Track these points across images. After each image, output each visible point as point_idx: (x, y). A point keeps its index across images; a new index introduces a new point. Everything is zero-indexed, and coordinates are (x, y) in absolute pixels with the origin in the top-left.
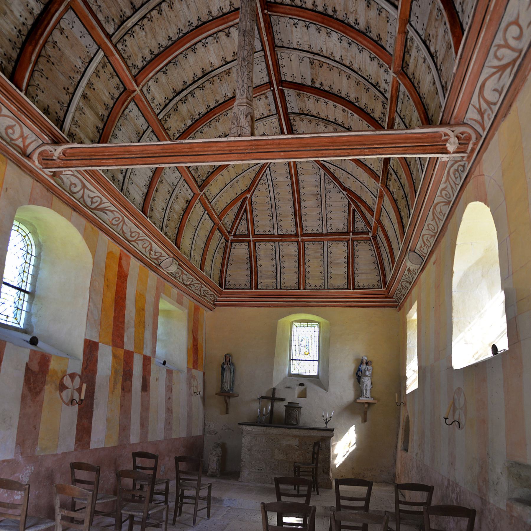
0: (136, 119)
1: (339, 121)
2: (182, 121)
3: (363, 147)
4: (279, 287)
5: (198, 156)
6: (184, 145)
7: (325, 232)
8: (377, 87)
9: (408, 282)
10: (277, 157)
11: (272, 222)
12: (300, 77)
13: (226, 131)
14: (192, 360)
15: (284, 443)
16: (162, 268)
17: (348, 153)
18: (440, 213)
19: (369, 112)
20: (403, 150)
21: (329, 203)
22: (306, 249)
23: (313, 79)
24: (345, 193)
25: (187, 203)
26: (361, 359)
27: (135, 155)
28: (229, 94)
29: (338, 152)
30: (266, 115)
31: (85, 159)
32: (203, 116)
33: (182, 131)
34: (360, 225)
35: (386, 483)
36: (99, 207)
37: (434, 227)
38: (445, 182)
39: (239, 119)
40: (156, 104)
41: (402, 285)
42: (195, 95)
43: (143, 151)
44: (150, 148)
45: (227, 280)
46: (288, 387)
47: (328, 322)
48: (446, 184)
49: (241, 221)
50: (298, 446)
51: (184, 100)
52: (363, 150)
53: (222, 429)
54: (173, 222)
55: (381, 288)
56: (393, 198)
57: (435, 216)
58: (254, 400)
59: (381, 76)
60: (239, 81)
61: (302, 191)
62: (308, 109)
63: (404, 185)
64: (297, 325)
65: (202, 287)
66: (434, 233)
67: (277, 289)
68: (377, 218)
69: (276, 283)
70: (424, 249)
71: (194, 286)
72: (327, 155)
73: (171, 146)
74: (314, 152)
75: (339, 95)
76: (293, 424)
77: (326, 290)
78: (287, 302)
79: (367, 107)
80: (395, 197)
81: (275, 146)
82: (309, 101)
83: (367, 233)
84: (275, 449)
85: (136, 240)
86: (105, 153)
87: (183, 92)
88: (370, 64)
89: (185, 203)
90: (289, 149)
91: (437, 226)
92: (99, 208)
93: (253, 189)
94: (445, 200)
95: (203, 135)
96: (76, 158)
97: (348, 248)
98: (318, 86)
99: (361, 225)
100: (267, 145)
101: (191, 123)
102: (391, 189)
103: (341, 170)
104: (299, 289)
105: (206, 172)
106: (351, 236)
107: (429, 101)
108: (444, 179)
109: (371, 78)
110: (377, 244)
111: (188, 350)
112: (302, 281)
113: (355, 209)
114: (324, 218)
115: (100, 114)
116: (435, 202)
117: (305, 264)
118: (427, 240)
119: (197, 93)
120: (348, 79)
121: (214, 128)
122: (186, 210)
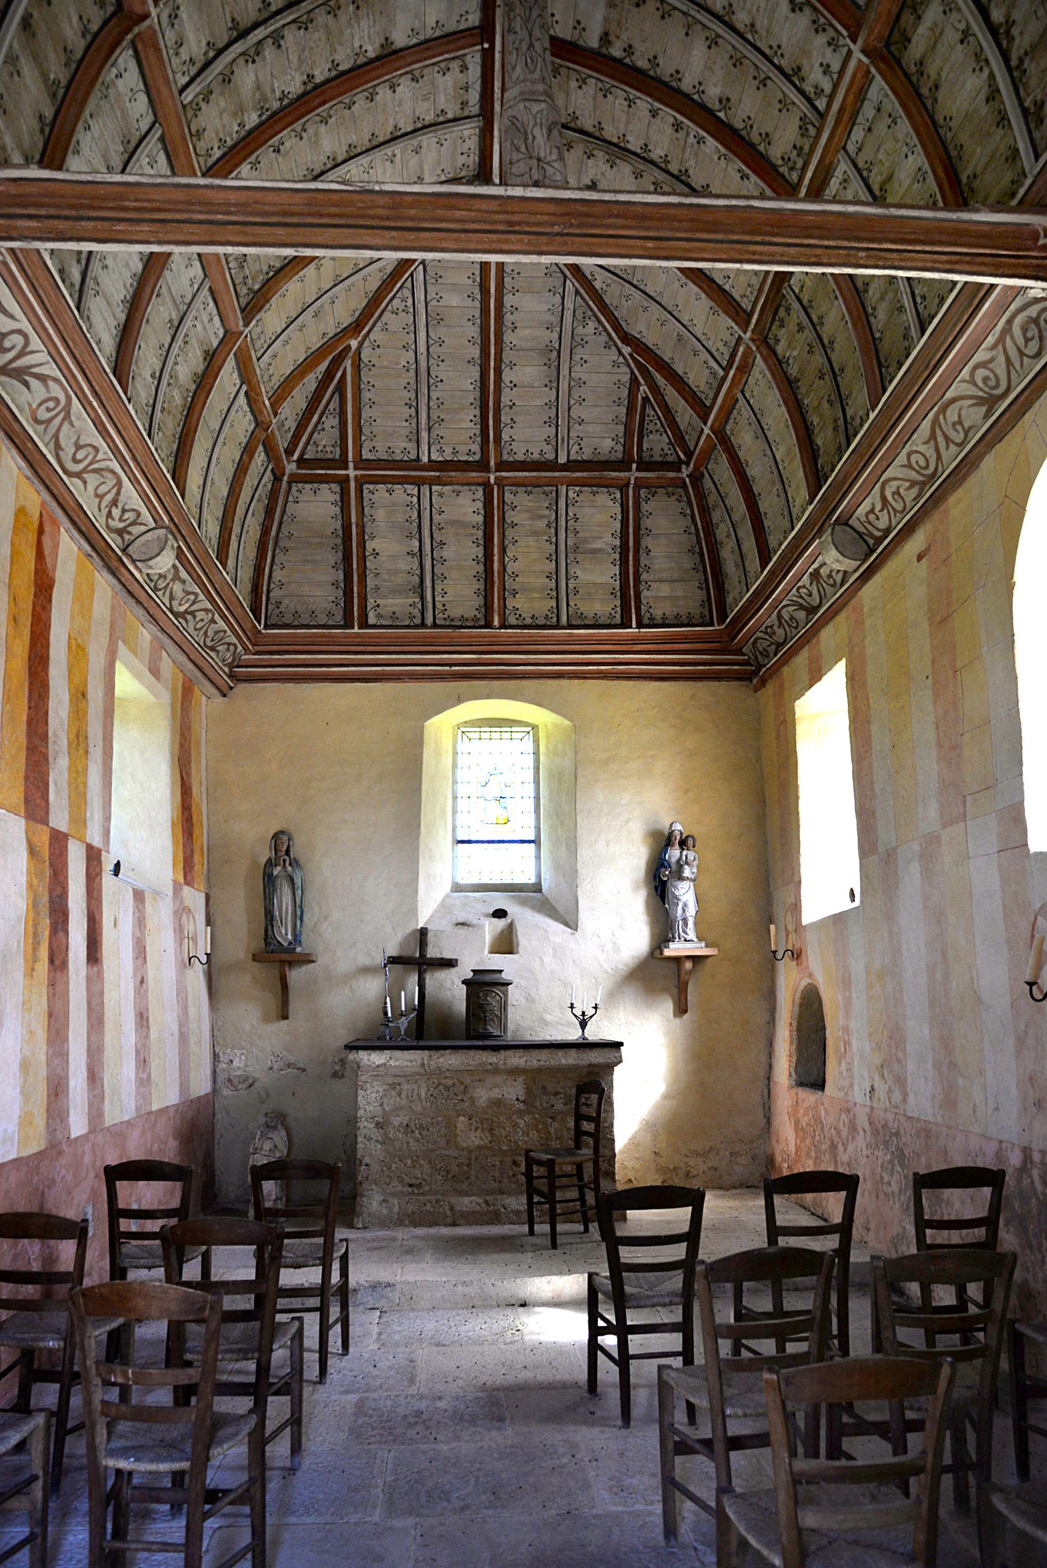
0: (127, 100)
1: (657, 154)
2: (235, 114)
3: (857, 245)
4: (429, 621)
5: (417, 233)
6: (375, 196)
7: (562, 459)
8: (795, 80)
9: (801, 607)
10: (635, 253)
11: (414, 425)
12: (571, 22)
13: (339, 152)
14: (181, 858)
15: (483, 1095)
16: (133, 561)
17: (817, 256)
18: (954, 424)
19: (755, 138)
20: (947, 262)
21: (578, 375)
22: (506, 508)
23: (606, 34)
24: (626, 350)
25: (205, 359)
26: (666, 832)
27: (224, 214)
28: (370, 48)
29: (792, 250)
30: (450, 116)
31: (58, 217)
32: (290, 104)
33: (229, 143)
34: (658, 443)
35: (742, 1186)
36: (14, 365)
37: (927, 461)
38: (994, 347)
39: (530, 137)
40: (184, 58)
41: (780, 616)
42: (282, 43)
43: (246, 205)
44: (270, 197)
45: (272, 600)
46: (463, 924)
47: (567, 722)
48: (994, 352)
49: (324, 419)
50: (523, 1102)
51: (251, 57)
52: (853, 252)
53: (271, 1069)
54: (171, 417)
55: (713, 625)
56: (785, 373)
57: (938, 431)
58: (367, 970)
59: (815, 53)
60: (518, 29)
61: (508, 337)
62: (570, 111)
63: (831, 343)
64: (471, 735)
65: (213, 621)
66: (923, 475)
67: (423, 625)
68: (716, 426)
69: (419, 606)
70: (878, 519)
71: (195, 617)
72: (765, 258)
73: (335, 197)
74: (734, 246)
75: (674, 84)
76: (489, 1036)
77: (563, 628)
78: (451, 665)
79: (751, 127)
80: (793, 371)
81: (629, 222)
82: (579, 92)
83: (676, 466)
84: (458, 1116)
85: (84, 470)
86: (126, 203)
87: (256, 32)
88: (787, 18)
89: (201, 359)
90: (669, 234)
91: (939, 457)
92: (14, 369)
93: (371, 323)
94: (981, 394)
95: (280, 159)
96: (31, 211)
97: (622, 506)
98: (616, 52)
99: (660, 442)
100: (610, 217)
101: (257, 121)
102: (780, 349)
103: (627, 285)
104: (488, 625)
105: (265, 269)
106: (634, 474)
107: (964, 138)
108: (990, 340)
109: (782, 55)
110: (701, 496)
111: (173, 825)
112: (496, 601)
113: (647, 396)
114: (563, 417)
115: (52, 77)
116: (949, 395)
117: (503, 550)
118: (897, 493)
119: (292, 36)
120: (709, 47)
121: (310, 140)
122: (205, 381)
